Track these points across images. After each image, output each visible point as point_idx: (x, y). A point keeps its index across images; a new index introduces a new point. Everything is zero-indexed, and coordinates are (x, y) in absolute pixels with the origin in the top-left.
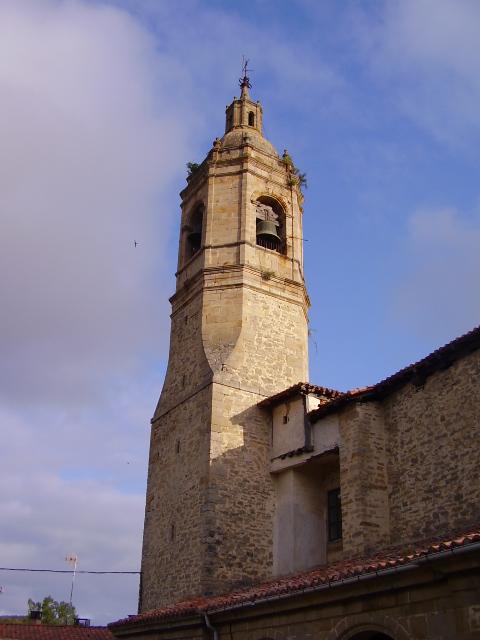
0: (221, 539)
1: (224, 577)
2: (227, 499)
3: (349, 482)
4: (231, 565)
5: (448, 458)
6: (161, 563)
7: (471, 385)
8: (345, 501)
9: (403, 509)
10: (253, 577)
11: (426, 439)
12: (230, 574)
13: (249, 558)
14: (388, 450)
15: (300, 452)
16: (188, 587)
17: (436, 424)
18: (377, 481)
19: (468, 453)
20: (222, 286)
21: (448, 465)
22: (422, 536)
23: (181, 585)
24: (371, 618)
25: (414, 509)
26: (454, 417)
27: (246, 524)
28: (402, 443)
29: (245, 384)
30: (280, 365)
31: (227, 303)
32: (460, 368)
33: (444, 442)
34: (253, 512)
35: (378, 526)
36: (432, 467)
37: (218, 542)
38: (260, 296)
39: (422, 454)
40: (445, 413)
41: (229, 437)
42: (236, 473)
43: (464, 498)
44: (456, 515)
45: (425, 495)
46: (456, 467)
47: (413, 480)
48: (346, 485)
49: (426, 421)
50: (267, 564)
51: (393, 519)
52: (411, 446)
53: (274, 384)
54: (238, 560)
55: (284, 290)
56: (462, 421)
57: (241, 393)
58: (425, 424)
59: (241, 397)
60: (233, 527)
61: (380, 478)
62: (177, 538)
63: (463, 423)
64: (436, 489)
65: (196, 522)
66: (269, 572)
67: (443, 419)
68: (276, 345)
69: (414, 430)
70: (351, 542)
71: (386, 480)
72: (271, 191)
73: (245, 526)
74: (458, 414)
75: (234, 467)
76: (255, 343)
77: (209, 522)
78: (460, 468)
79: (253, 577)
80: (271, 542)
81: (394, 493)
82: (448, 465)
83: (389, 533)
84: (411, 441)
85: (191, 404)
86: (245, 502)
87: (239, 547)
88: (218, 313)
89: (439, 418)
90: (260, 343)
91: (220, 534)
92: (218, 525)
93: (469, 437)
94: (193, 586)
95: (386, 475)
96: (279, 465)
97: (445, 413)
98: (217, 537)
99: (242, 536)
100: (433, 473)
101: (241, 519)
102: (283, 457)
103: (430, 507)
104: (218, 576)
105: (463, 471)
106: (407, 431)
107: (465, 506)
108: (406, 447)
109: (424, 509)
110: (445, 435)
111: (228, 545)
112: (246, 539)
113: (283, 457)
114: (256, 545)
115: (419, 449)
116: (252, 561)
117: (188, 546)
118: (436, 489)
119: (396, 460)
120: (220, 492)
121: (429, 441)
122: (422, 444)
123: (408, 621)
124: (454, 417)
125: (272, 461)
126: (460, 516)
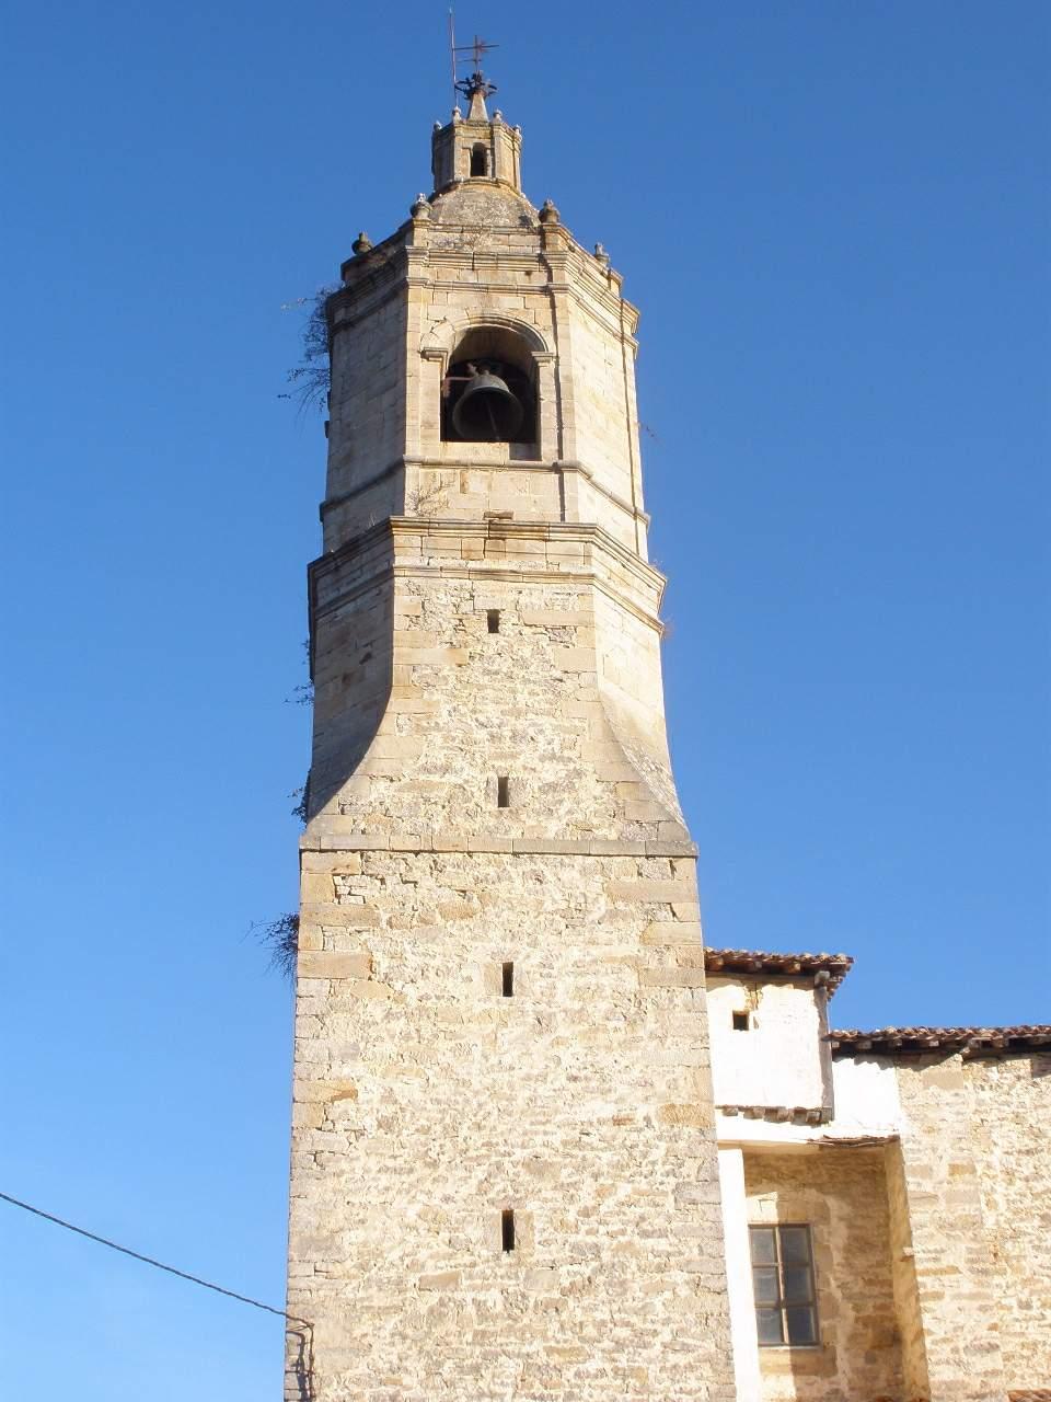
9: (1017, 1313)
15: (801, 1116)
106: (1028, 1152)
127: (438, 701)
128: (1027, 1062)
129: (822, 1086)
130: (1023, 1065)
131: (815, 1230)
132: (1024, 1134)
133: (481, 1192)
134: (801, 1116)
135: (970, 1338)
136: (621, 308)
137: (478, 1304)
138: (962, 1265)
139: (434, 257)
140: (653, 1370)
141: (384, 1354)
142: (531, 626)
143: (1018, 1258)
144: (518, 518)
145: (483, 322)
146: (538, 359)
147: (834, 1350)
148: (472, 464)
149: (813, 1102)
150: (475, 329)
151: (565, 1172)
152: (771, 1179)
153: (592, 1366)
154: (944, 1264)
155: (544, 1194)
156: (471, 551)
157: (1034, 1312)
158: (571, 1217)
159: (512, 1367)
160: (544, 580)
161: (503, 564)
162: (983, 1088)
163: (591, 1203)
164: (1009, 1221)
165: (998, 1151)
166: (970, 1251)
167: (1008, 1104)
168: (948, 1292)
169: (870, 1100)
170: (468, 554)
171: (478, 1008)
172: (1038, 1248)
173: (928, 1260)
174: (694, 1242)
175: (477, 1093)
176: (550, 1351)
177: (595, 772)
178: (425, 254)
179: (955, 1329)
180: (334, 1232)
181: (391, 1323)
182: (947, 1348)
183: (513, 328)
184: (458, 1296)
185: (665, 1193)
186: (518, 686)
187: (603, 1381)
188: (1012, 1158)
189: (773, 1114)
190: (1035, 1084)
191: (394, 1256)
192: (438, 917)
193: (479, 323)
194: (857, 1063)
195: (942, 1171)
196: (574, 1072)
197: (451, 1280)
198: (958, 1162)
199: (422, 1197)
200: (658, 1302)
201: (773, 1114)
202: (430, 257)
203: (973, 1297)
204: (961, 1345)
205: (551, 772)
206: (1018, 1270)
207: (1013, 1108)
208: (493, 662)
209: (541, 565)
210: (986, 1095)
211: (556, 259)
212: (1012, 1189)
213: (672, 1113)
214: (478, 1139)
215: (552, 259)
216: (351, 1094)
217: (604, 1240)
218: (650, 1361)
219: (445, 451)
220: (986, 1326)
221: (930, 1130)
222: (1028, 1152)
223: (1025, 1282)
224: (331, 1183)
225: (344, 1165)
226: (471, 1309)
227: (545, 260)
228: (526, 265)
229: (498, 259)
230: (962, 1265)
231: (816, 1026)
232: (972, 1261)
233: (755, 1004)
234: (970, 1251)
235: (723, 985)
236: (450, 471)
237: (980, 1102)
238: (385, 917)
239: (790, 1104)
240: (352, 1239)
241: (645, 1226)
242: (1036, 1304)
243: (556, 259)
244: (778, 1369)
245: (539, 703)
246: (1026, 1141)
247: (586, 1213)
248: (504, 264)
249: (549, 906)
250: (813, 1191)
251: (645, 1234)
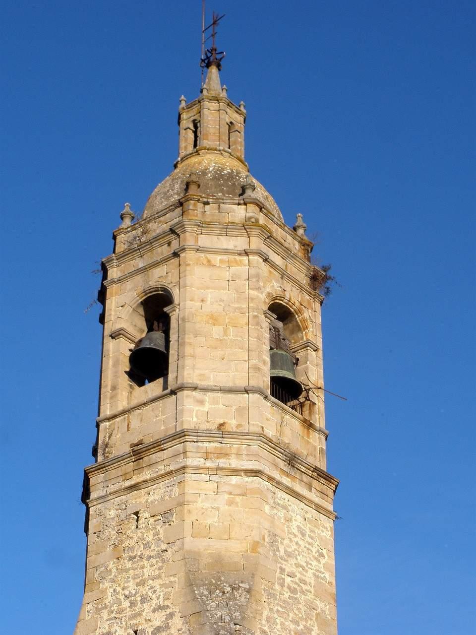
127: (106, 588)
136: (245, 229)
139: (119, 259)
142: (154, 516)
144: (148, 441)
145: (146, 294)
146: (168, 312)
148: (132, 409)
150: (144, 300)
156: (126, 474)
160: (160, 480)
161: (147, 475)
177: (179, 612)
178: (113, 260)
183: (161, 291)
186: (145, 563)
192: (263, 592)
193: (145, 295)
202: (117, 259)
208: (133, 550)
209: (161, 469)
211: (179, 227)
215: (177, 229)
227: (174, 231)
228: (167, 239)
229: (151, 243)
236: (122, 417)
243: (179, 227)
245: (154, 571)
248: (156, 244)
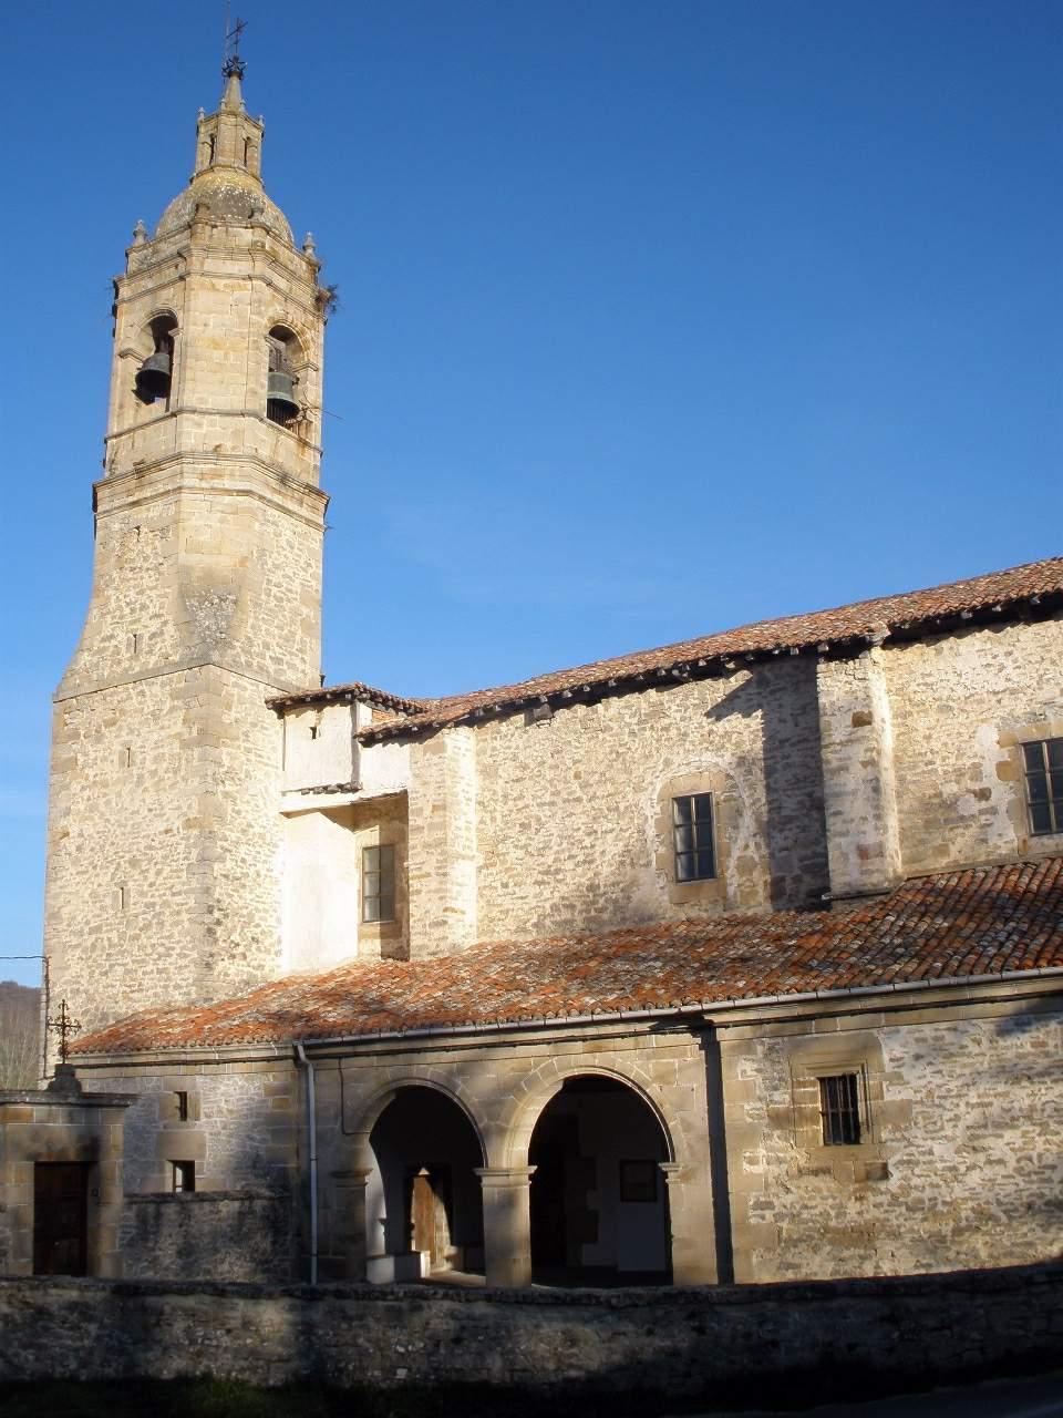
0: (221, 917)
1: (226, 975)
2: (228, 854)
3: (427, 845)
4: (233, 957)
5: (581, 832)
6: (94, 946)
7: (626, 739)
8: (415, 873)
9: (500, 891)
10: (258, 973)
11: (547, 798)
12: (232, 971)
13: (254, 946)
14: (480, 803)
15: (342, 788)
16: (166, 987)
17: (566, 782)
18: (464, 847)
19: (612, 831)
20: (213, 489)
21: (581, 842)
22: (530, 932)
23: (147, 982)
24: (597, 1059)
25: (519, 894)
26: (596, 777)
27: (250, 893)
28: (505, 796)
29: (249, 665)
30: (293, 634)
31: (222, 521)
32: (612, 711)
33: (579, 809)
34: (258, 875)
35: (463, 913)
36: (555, 840)
37: (219, 923)
38: (273, 513)
39: (539, 819)
40: (582, 768)
41: (229, 754)
42: (238, 812)
43: (602, 890)
44: (588, 911)
45: (540, 878)
46: (593, 846)
47: (520, 853)
48: (419, 849)
49: (549, 774)
50: (276, 954)
51: (482, 903)
52: (520, 804)
53: (285, 667)
54: (241, 949)
55: (301, 503)
56: (609, 785)
57: (244, 682)
58: (548, 777)
59: (245, 689)
60: (236, 899)
61: (468, 843)
62: (132, 910)
63: (610, 788)
64: (558, 871)
65: (178, 888)
66: (278, 967)
67: (577, 776)
68: (289, 600)
69: (528, 783)
70: (425, 934)
71: (474, 845)
72: (290, 318)
73: (249, 897)
74: (603, 774)
75: (235, 804)
76: (263, 597)
77: (207, 891)
78: (598, 849)
79: (258, 973)
80: (279, 920)
81: (486, 866)
82: (581, 842)
83: (475, 923)
84: (521, 797)
85: (156, 689)
86: (249, 860)
87: (243, 928)
88: (205, 537)
89: (572, 773)
90: (269, 596)
91: (220, 910)
92: (216, 896)
93: (617, 809)
94: (177, 987)
95: (474, 839)
96: (296, 802)
97: (582, 768)
98: (217, 914)
99: (245, 912)
100: (556, 848)
101: (244, 886)
102: (305, 792)
103: (547, 894)
104: (220, 974)
105: (603, 852)
106: (518, 781)
107: (602, 901)
108: (511, 803)
109: (535, 896)
110: (578, 800)
111: (230, 925)
112: (250, 915)
113: (305, 792)
114: (262, 923)
115: (535, 811)
116: (258, 949)
117: (161, 924)
118: (558, 871)
119: (493, 819)
120: (219, 843)
121: (552, 804)
122: (541, 805)
123: (651, 1066)
124: (596, 777)
125: (284, 794)
126: (593, 913)
128: (522, 716)
129: (351, 768)
130: (520, 718)
131: (397, 847)
132: (517, 767)
133: (112, 879)
134: (342, 788)
135: (432, 917)
137: (109, 939)
138: (433, 871)
140: (172, 969)
141: (75, 969)
143: (503, 854)
147: (401, 922)
149: (346, 779)
151: (144, 863)
152: (375, 817)
153: (148, 969)
154: (423, 872)
155: (136, 877)
157: (510, 890)
158: (145, 888)
159: (119, 970)
162: (496, 739)
163: (153, 880)
164: (502, 830)
165: (501, 782)
166: (438, 861)
167: (509, 748)
168: (424, 889)
169: (386, 770)
170: (129, 493)
171: (115, 776)
172: (516, 847)
173: (415, 869)
174: (192, 897)
175: (113, 825)
176: (133, 961)
179: (426, 912)
180: (59, 908)
181: (78, 953)
182: (420, 924)
184: (101, 936)
185: (182, 870)
187: (152, 976)
188: (508, 785)
189: (326, 790)
190: (526, 732)
191: (79, 918)
194: (401, 746)
195: (427, 812)
196: (150, 807)
197: (98, 929)
198: (436, 803)
199: (90, 886)
200: (176, 932)
201: (326, 790)
203: (437, 891)
204: (428, 922)
205: (154, 626)
206: (503, 862)
207: (512, 750)
210: (497, 743)
212: (506, 807)
213: (189, 824)
214: (112, 851)
216: (67, 834)
217: (157, 900)
218: (170, 964)
219: (151, 411)
220: (442, 909)
221: (425, 783)
222: (518, 781)
223: (507, 870)
224: (59, 883)
225: (64, 873)
226: (106, 943)
230: (433, 871)
231: (350, 730)
232: (439, 868)
233: (319, 719)
234: (438, 861)
235: (305, 711)
237: (494, 749)
238: (83, 733)
239: (333, 783)
240: (65, 912)
241: (174, 890)
242: (511, 885)
244: (372, 936)
246: (518, 772)
247: (151, 885)
249: (146, 710)
250: (397, 822)
251: (174, 894)
